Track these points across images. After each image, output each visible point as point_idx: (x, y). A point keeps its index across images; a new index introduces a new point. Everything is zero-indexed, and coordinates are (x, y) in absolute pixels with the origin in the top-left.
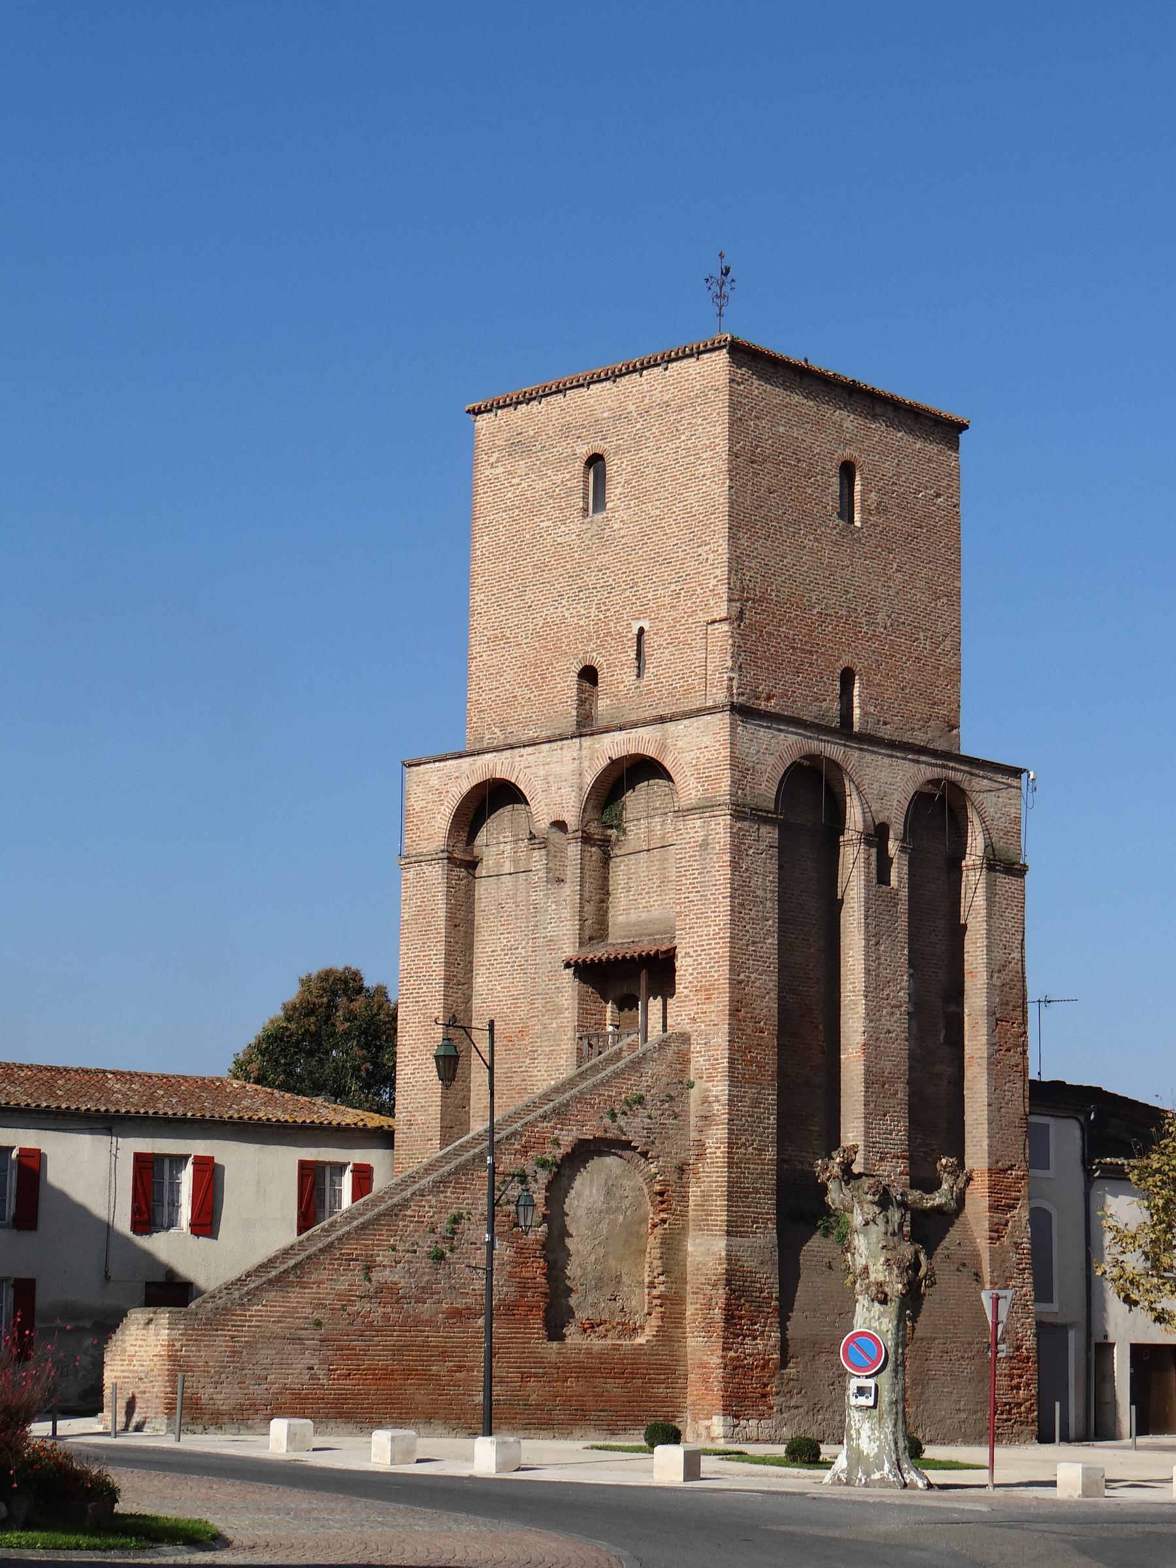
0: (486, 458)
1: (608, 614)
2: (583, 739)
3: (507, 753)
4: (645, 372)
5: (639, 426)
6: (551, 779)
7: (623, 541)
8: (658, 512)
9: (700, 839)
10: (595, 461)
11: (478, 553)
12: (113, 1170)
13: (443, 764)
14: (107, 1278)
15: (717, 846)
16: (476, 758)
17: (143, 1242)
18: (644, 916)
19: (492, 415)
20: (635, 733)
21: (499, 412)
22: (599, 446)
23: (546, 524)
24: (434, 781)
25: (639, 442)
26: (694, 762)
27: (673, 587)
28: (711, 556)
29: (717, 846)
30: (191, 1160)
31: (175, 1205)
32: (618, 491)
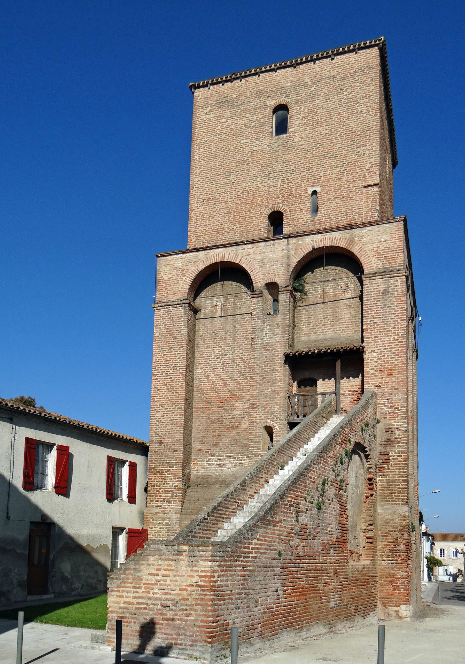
0: (202, 110)
1: (290, 184)
2: (290, 239)
3: (233, 248)
4: (317, 62)
5: (313, 89)
6: (266, 261)
7: (301, 147)
8: (327, 132)
9: (382, 290)
10: (282, 108)
11: (196, 157)
12: (13, 447)
13: (184, 255)
14: (8, 518)
15: (396, 293)
16: (209, 251)
17: (29, 495)
18: (321, 337)
19: (206, 89)
20: (328, 235)
21: (211, 87)
22: (283, 100)
23: (245, 141)
24: (179, 264)
25: (313, 97)
26: (375, 249)
27: (338, 169)
28: (367, 152)
29: (396, 293)
30: (55, 447)
31: (44, 474)
32: (297, 122)
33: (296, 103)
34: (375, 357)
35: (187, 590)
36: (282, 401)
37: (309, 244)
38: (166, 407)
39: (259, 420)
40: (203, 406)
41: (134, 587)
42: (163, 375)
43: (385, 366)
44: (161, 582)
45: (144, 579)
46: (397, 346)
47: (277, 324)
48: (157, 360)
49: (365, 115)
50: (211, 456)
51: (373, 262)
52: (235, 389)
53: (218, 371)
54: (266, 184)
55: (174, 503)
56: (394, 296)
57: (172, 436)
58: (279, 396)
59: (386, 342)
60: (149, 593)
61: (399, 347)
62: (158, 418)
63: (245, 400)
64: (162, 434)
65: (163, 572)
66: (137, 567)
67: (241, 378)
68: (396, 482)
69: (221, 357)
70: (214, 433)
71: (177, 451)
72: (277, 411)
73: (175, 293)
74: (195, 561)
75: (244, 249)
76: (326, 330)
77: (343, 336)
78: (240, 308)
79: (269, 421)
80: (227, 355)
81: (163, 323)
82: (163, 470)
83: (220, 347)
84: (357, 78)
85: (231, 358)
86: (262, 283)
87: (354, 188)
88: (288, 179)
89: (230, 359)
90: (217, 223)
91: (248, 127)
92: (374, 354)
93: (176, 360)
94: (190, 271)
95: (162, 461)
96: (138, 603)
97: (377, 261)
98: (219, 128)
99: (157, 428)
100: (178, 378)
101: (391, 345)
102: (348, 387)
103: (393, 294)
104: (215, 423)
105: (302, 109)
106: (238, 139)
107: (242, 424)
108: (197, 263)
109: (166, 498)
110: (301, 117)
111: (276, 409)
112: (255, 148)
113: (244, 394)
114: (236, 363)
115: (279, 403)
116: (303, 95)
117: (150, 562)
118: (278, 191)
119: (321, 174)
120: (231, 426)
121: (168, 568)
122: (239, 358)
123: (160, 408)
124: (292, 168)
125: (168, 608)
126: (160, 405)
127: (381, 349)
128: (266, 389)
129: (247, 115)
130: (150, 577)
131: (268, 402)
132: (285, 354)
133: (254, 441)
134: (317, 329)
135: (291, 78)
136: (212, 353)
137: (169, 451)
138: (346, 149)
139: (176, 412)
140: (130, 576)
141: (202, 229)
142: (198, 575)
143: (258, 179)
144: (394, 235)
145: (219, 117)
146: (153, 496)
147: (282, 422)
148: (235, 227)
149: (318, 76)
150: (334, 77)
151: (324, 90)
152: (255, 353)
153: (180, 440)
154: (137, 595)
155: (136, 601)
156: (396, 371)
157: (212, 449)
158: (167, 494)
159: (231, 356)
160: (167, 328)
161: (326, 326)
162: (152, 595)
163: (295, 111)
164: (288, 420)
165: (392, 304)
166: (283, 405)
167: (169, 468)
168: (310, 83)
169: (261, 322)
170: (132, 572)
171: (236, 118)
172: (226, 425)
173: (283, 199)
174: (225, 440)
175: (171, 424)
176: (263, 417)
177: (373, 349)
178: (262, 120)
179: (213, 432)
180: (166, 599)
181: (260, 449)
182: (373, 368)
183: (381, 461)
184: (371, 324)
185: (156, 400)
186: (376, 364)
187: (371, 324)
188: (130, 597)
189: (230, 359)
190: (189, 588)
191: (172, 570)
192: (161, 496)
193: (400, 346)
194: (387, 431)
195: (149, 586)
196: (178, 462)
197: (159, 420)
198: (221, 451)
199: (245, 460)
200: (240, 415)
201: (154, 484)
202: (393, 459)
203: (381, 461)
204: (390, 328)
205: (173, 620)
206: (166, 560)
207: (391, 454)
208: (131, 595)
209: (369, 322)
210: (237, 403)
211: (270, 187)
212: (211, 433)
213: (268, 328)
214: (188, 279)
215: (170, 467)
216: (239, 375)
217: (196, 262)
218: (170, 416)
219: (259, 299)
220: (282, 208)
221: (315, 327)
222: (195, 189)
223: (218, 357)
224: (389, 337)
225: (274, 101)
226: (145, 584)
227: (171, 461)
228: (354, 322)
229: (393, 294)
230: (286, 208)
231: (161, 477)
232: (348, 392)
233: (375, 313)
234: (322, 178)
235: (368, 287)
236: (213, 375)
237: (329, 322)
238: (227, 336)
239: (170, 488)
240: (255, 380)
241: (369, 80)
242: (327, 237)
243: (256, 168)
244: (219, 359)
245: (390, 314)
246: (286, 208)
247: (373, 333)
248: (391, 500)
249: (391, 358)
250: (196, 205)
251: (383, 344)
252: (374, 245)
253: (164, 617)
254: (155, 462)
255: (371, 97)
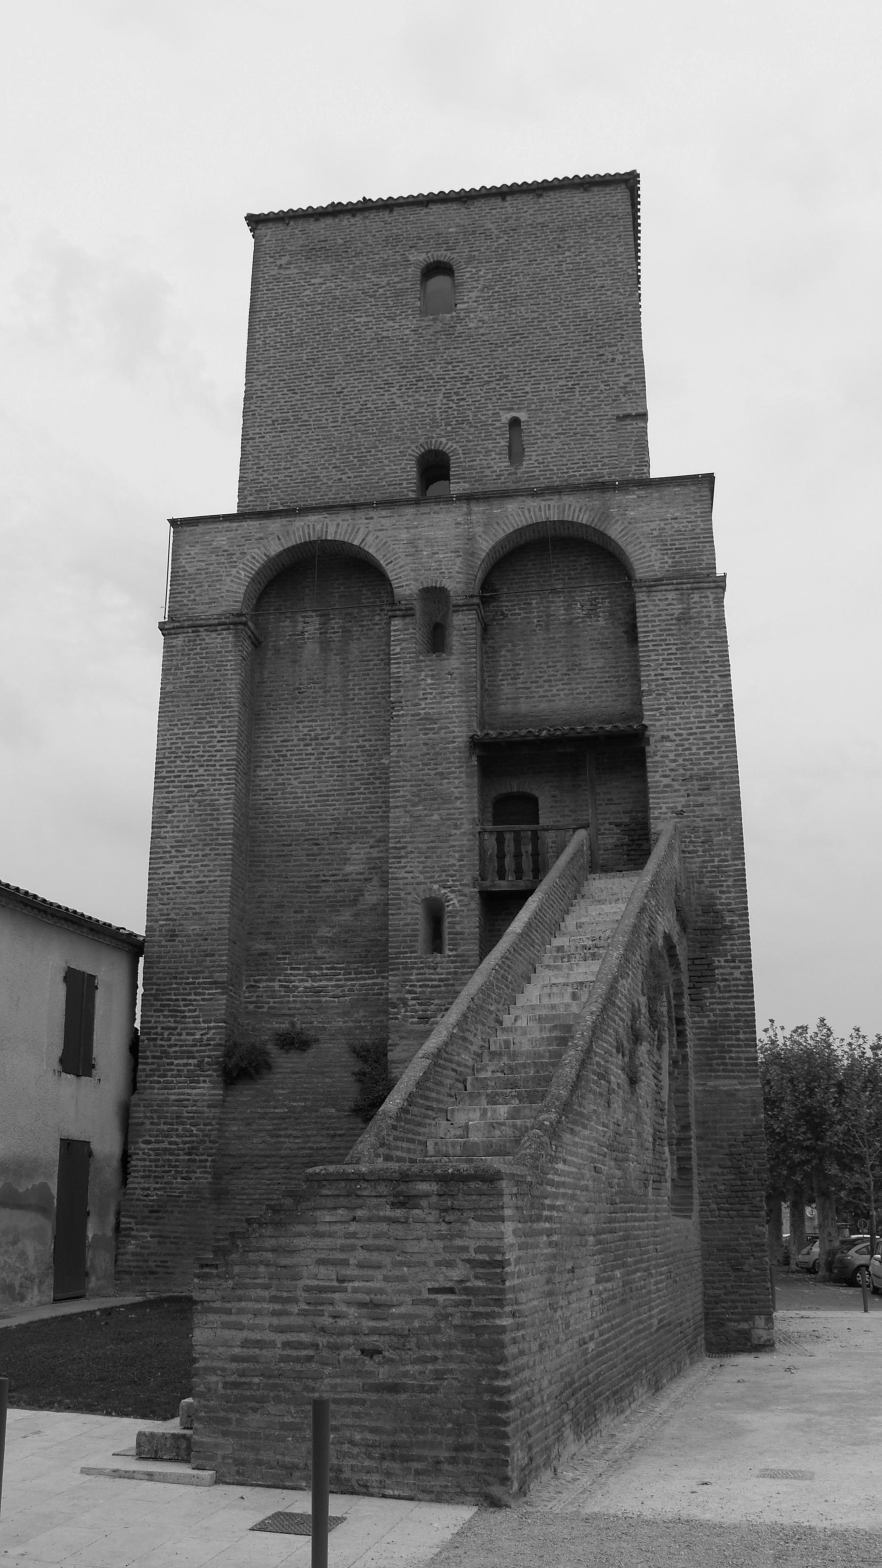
1: (462, 403)
5: (501, 241)
6: (421, 544)
7: (484, 338)
8: (535, 315)
9: (677, 612)
15: (706, 621)
18: (543, 706)
22: (442, 255)
23: (363, 320)
26: (655, 533)
28: (619, 357)
29: (706, 621)
33: (469, 262)
34: (672, 751)
35: (434, 1303)
36: (465, 842)
37: (518, 515)
38: (187, 852)
39: (412, 884)
40: (271, 851)
41: (274, 1299)
42: (182, 778)
43: (692, 769)
44: (356, 1284)
45: (305, 1273)
46: (716, 730)
47: (450, 674)
48: (168, 745)
49: (609, 293)
50: (292, 969)
51: (653, 557)
52: (349, 815)
53: (307, 773)
54: (410, 400)
55: (204, 1082)
56: (701, 626)
57: (202, 919)
58: (458, 832)
59: (692, 720)
60: (321, 1314)
61: (721, 732)
62: (167, 876)
63: (372, 841)
64: (177, 914)
65: (362, 1255)
66: (283, 1241)
67: (362, 790)
68: (730, 1027)
69: (313, 743)
70: (299, 916)
71: (213, 955)
72: (454, 865)
73: (212, 601)
74: (459, 1221)
75: (372, 518)
76: (554, 692)
77: (591, 705)
78: (358, 639)
79: (436, 887)
80: (328, 738)
81: (183, 664)
82: (177, 1000)
83: (312, 721)
84: (589, 231)
85: (338, 745)
86: (412, 587)
87: (597, 419)
88: (457, 394)
89: (336, 748)
90: (305, 467)
91: (371, 296)
92: (668, 744)
93: (214, 746)
94: (249, 557)
95: (176, 978)
96: (286, 1345)
97: (660, 556)
98: (307, 292)
99: (165, 901)
100: (216, 787)
101: (704, 727)
102: (608, 816)
103: (700, 623)
104: (303, 892)
105: (481, 273)
106: (348, 315)
107: (366, 894)
108: (265, 542)
109: (185, 1069)
110: (480, 287)
111: (452, 861)
112: (385, 334)
113: (369, 826)
114: (351, 757)
115: (459, 846)
116: (482, 249)
117: (322, 1228)
118: (438, 414)
119: (527, 389)
120: (339, 898)
121: (378, 1242)
122: (358, 747)
123: (174, 853)
124: (466, 373)
125: (377, 1358)
126: (172, 847)
127: (681, 735)
128: (426, 816)
129: (368, 275)
130: (323, 1271)
131: (432, 845)
132: (472, 737)
133: (401, 934)
134: (533, 689)
135: (457, 220)
136: (294, 733)
137: (193, 956)
138: (576, 348)
139: (212, 864)
140: (262, 1269)
141: (271, 477)
142: (468, 1261)
143: (393, 390)
144: (693, 509)
145: (306, 273)
146: (152, 1064)
147: (467, 890)
148: (344, 477)
149: (511, 221)
150: (543, 225)
151: (524, 245)
152: (400, 736)
153: (220, 929)
154: (285, 1321)
155: (280, 1338)
156: (718, 782)
157: (293, 952)
158: (188, 1058)
159: (337, 742)
160: (193, 674)
161: (553, 683)
162: (331, 1320)
163: (468, 275)
164: (480, 885)
165: (699, 642)
166: (468, 851)
167: (193, 997)
168: (496, 232)
169: (412, 668)
170: (270, 1255)
171: (344, 278)
172: (328, 897)
173: (449, 428)
174: (324, 931)
175: (199, 892)
176: (421, 878)
177: (666, 733)
178: (399, 286)
179: (295, 912)
180: (374, 1331)
181: (416, 952)
182: (668, 773)
183: (696, 979)
184: (657, 680)
185: (162, 835)
186: (673, 765)
187: (657, 680)
188: (261, 1328)
189: (336, 748)
190: (441, 1298)
191: (389, 1250)
192: (172, 1064)
193: (722, 728)
194: (706, 912)
195: (319, 1296)
196: (215, 983)
197: (171, 881)
198: (315, 958)
199: (373, 978)
200: (361, 874)
201: (156, 1034)
202: (722, 974)
203: (696, 979)
204: (699, 691)
205: (394, 1388)
206: (370, 1220)
207: (717, 963)
208: (266, 1321)
209: (653, 678)
210: (354, 846)
211: (419, 404)
212: (292, 914)
213: (429, 681)
214: (243, 573)
215: (196, 994)
216: (357, 784)
217: (262, 538)
218: (197, 873)
219: (408, 620)
220: (447, 445)
221: (529, 685)
222: (255, 400)
223: (307, 742)
224: (698, 710)
225: (424, 255)
226: (308, 1289)
227: (198, 978)
228: (615, 677)
229: (700, 623)
230: (455, 446)
231: (172, 1016)
232: (607, 826)
233: (664, 660)
234: (529, 396)
235: (645, 606)
236: (295, 783)
237: (559, 676)
238: (328, 698)
239: (195, 1045)
240: (402, 793)
241: (613, 236)
242: (552, 503)
243: (388, 369)
244: (309, 748)
245: (695, 663)
246: (455, 446)
247: (663, 701)
248: (721, 1068)
249: (705, 754)
250: (257, 430)
251: (687, 723)
252: (653, 525)
253: (370, 1381)
254: (159, 982)
255: (620, 265)
